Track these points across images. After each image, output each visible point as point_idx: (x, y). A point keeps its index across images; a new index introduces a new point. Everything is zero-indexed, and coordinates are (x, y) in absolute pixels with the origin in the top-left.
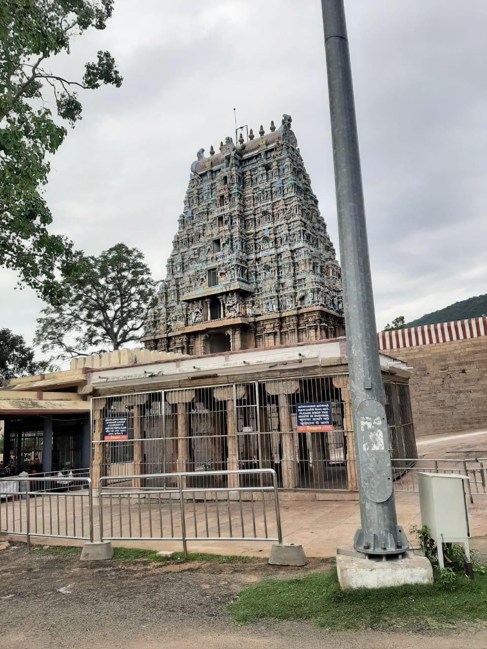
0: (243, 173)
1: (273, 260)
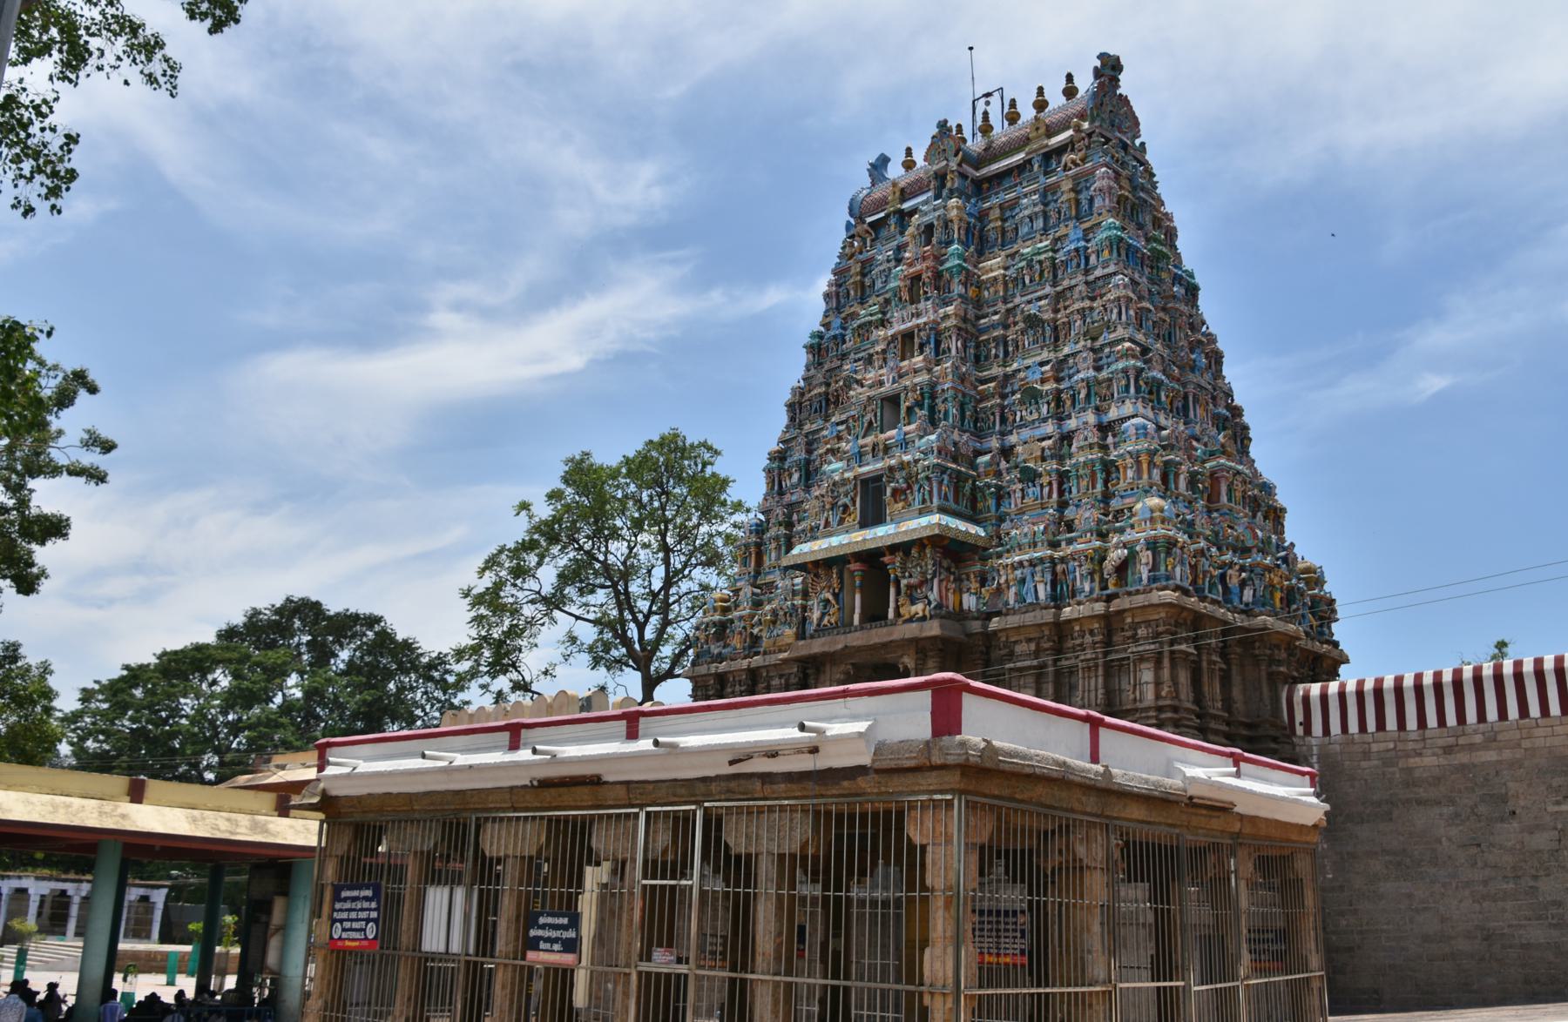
0: (982, 216)
1: (1047, 453)
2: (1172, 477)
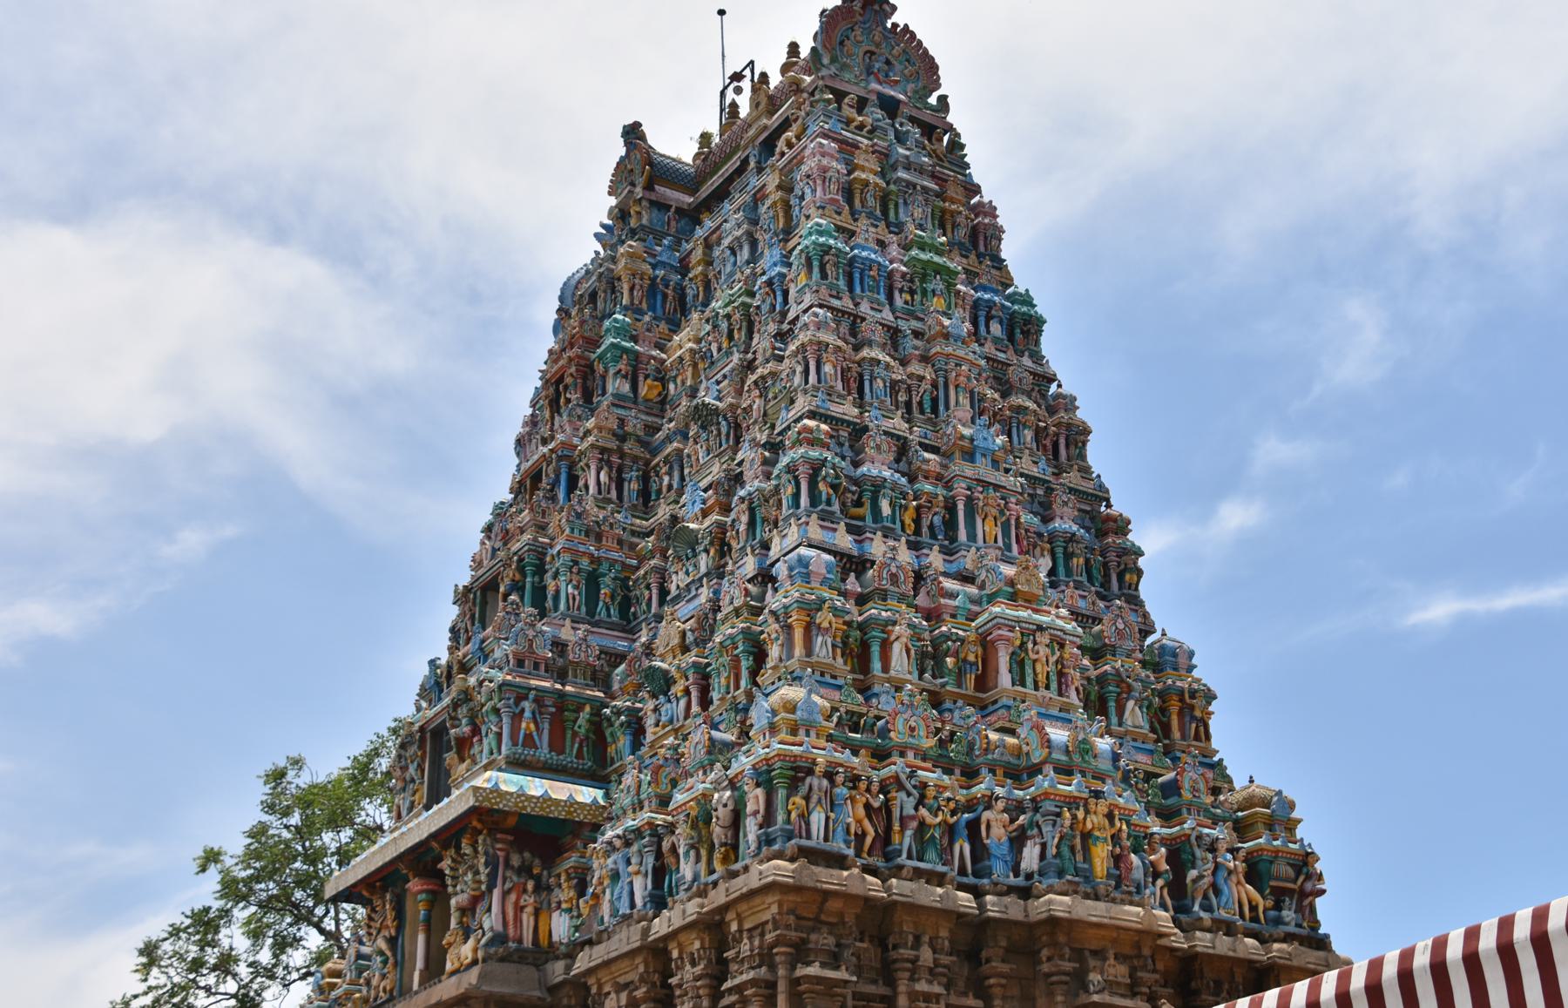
1: (690, 637)
2: (875, 649)
